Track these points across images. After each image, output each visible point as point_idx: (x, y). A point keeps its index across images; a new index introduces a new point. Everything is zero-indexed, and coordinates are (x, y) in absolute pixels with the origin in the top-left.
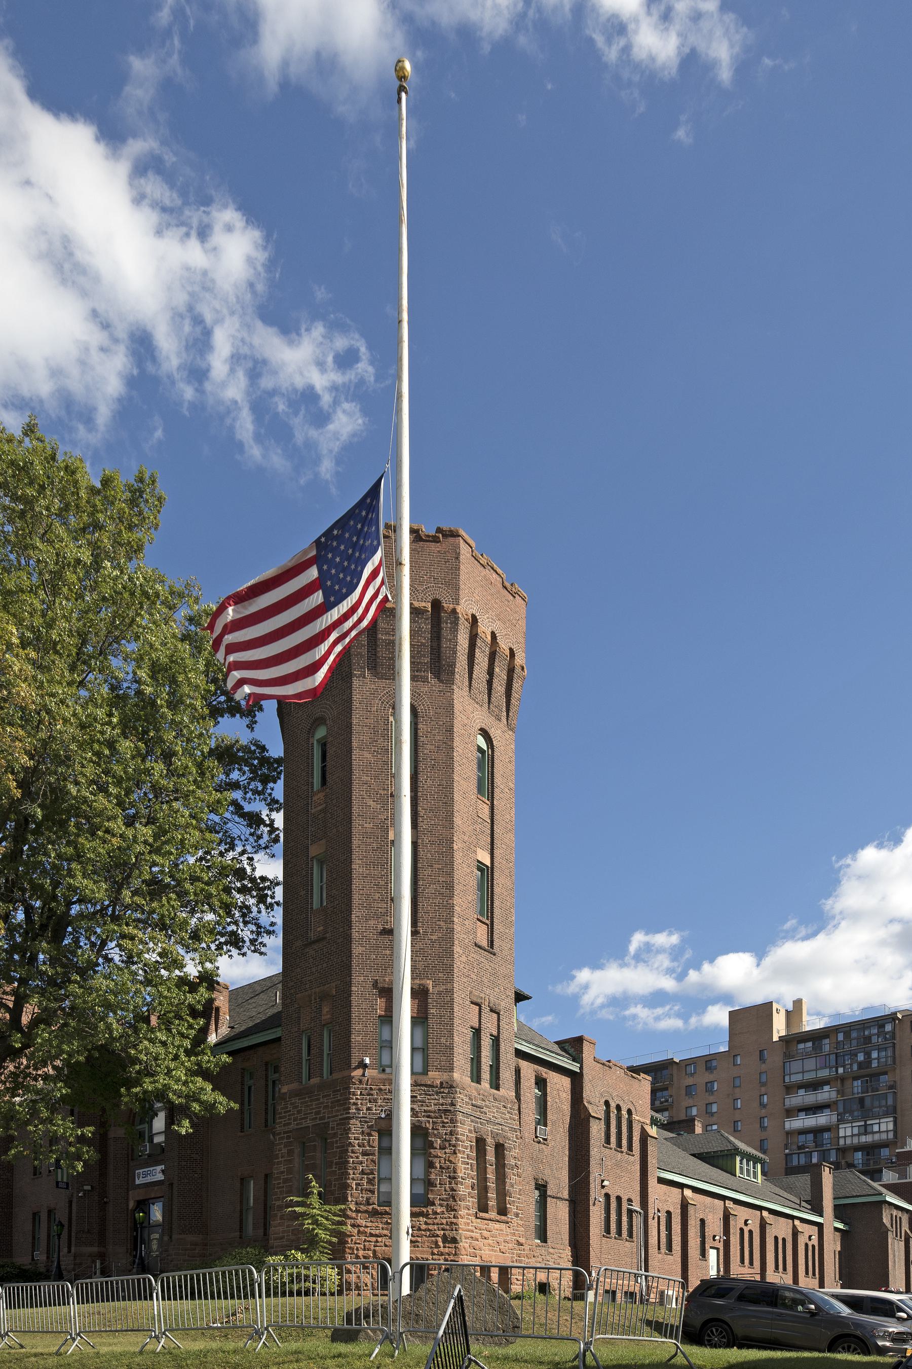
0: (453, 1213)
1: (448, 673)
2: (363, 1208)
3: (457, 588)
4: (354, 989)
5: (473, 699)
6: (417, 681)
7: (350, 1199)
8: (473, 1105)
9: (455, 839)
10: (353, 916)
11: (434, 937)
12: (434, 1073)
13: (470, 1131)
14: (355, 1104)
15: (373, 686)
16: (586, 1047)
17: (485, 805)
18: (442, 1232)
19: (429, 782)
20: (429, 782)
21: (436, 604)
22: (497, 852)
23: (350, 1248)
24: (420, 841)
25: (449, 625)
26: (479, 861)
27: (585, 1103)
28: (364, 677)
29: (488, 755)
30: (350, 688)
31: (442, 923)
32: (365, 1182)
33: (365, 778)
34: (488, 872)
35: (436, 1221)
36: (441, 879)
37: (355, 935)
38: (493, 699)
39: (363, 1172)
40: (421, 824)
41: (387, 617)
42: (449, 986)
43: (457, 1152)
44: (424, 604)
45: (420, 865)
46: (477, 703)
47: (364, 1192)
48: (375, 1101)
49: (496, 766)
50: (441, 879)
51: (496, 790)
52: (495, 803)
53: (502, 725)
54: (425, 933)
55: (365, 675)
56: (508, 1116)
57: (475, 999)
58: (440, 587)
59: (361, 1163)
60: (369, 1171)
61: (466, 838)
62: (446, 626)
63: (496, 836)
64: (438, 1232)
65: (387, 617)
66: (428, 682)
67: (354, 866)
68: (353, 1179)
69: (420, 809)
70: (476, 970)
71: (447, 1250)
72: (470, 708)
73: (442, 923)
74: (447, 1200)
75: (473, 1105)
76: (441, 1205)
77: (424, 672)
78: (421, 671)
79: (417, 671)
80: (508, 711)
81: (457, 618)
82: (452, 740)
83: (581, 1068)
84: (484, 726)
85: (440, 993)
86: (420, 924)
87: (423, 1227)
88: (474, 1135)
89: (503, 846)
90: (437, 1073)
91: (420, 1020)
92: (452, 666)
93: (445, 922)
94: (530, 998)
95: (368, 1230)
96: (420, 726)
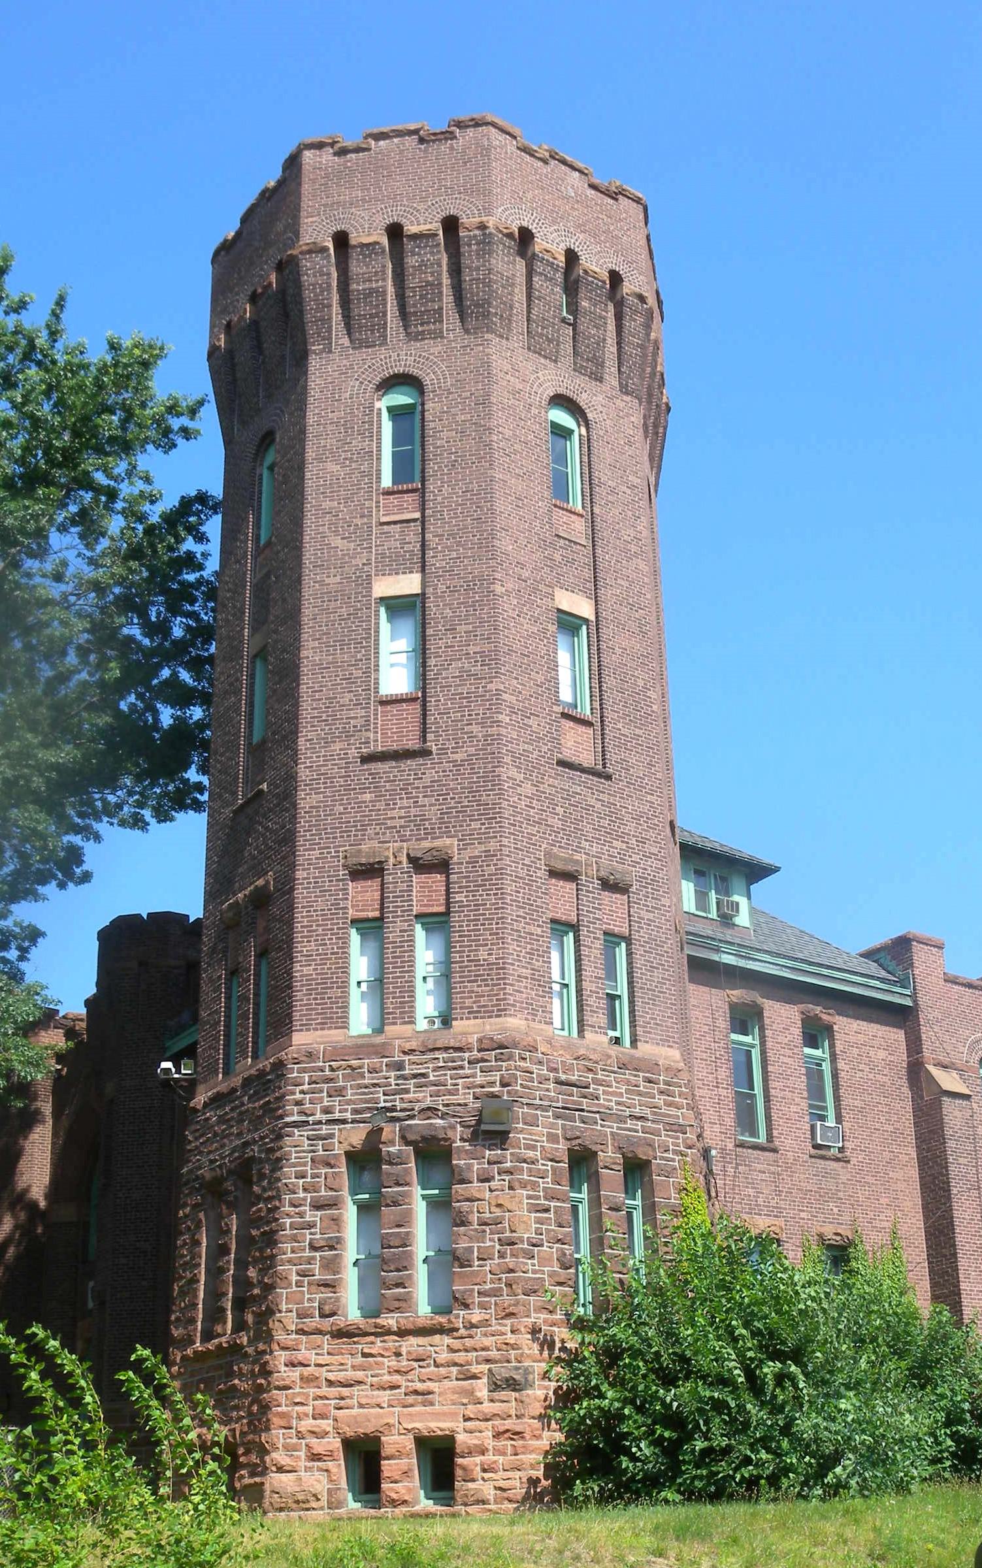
0: (508, 1322)
2: (315, 1322)
4: (300, 874)
5: (535, 352)
6: (423, 339)
7: (284, 1307)
8: (559, 1082)
10: (301, 741)
11: (458, 757)
12: (465, 1022)
13: (553, 1138)
14: (298, 1103)
15: (345, 362)
16: (920, 954)
18: (485, 1367)
20: (446, 490)
23: (282, 1415)
24: (429, 590)
25: (474, 247)
26: (559, 610)
27: (931, 1068)
28: (330, 352)
31: (475, 729)
32: (316, 1267)
33: (327, 504)
35: (468, 1342)
36: (472, 649)
37: (303, 773)
41: (365, 258)
42: (492, 845)
43: (516, 1185)
45: (429, 632)
46: (545, 357)
48: (340, 1092)
49: (595, 451)
53: (605, 387)
54: (443, 751)
56: (660, 1100)
57: (559, 866)
59: (311, 1226)
60: (322, 1243)
61: (526, 574)
63: (600, 566)
64: (475, 1369)
65: (365, 258)
66: (442, 337)
67: (304, 653)
70: (559, 810)
71: (496, 1407)
72: (530, 366)
73: (475, 729)
74: (496, 1293)
75: (559, 1082)
76: (484, 1306)
77: (434, 323)
78: (428, 323)
79: (422, 325)
83: (913, 997)
85: (473, 861)
86: (430, 736)
87: (444, 1356)
88: (562, 1146)
90: (472, 1022)
92: (482, 306)
93: (483, 724)
94: (777, 869)
95: (323, 1373)
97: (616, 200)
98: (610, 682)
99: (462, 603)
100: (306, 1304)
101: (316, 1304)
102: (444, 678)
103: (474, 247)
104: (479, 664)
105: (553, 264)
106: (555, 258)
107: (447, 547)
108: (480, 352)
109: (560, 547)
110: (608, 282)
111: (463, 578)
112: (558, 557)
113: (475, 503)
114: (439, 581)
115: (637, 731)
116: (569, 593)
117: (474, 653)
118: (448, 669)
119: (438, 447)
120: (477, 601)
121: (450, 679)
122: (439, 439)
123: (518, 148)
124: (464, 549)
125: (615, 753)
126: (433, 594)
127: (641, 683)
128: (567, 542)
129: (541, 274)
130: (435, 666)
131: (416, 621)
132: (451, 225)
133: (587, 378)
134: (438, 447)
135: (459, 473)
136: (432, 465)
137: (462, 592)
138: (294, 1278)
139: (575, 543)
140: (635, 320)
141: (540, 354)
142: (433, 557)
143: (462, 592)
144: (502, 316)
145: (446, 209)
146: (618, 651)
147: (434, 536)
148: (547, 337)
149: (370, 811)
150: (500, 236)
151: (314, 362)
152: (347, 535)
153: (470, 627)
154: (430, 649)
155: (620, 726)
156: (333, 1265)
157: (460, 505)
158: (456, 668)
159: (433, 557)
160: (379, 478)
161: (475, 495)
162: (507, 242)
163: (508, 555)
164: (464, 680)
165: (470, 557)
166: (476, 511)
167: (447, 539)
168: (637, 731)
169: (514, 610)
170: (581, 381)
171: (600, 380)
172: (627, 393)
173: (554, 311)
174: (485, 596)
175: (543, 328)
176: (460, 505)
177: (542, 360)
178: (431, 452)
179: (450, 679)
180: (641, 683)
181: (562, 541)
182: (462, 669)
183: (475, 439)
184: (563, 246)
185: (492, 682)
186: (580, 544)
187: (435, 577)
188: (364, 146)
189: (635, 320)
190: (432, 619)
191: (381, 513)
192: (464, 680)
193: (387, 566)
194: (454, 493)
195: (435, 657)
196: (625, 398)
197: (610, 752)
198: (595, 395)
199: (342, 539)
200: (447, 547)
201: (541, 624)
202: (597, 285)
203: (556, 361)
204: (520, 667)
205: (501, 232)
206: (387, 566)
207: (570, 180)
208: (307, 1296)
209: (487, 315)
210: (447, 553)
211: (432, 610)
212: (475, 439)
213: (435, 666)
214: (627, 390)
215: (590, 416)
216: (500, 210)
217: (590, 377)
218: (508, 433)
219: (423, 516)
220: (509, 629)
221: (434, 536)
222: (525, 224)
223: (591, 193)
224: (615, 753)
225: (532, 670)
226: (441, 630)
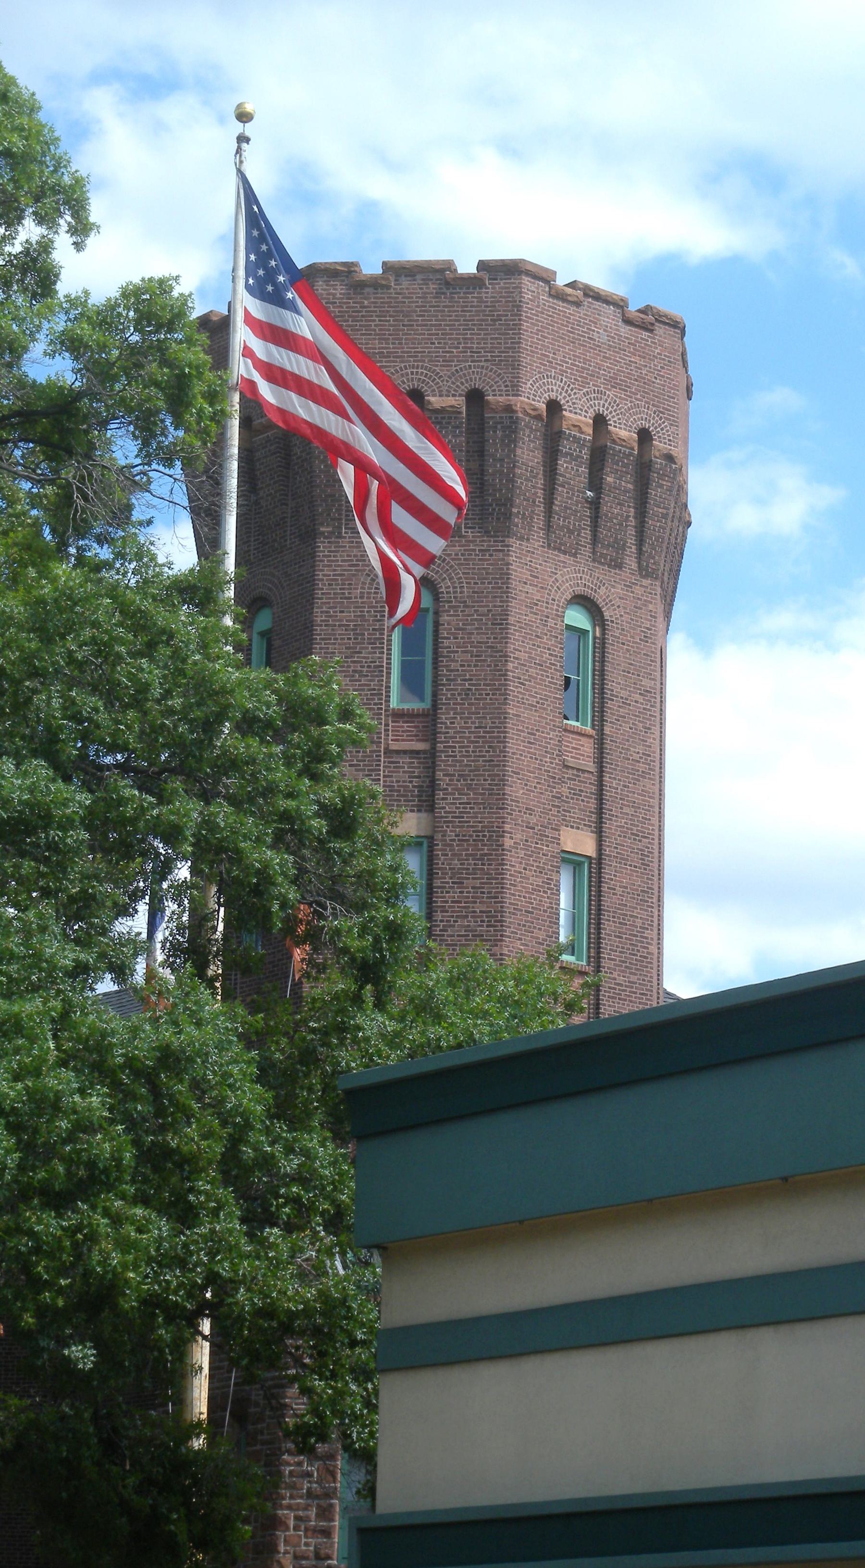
1: (498, 519)
3: (514, 365)
5: (555, 549)
7: (282, 1548)
9: (507, 827)
17: (584, 740)
19: (459, 723)
20: (459, 723)
21: (475, 397)
22: (611, 827)
24: (438, 836)
28: (340, 536)
29: (595, 638)
30: (313, 555)
32: (312, 1513)
34: (590, 868)
36: (478, 908)
38: (603, 532)
39: (310, 1494)
40: (442, 803)
44: (450, 401)
45: (437, 883)
46: (565, 553)
47: (310, 1533)
50: (478, 908)
51: (609, 704)
52: (607, 730)
53: (625, 574)
55: (340, 533)
58: (482, 367)
61: (533, 820)
62: (494, 438)
63: (607, 795)
66: (461, 536)
68: (289, 1507)
69: (440, 774)
80: (640, 542)
81: (515, 422)
82: (504, 639)
84: (580, 590)
89: (626, 810)
91: (272, 240)
96: (444, 618)
97: (651, 331)
98: (608, 927)
99: (471, 855)
100: (304, 1548)
101: (312, 1548)
102: (448, 936)
103: (499, 433)
104: (485, 924)
105: (580, 438)
106: (582, 433)
107: (457, 789)
108: (499, 560)
109: (568, 779)
110: (636, 448)
111: (472, 827)
112: (565, 791)
113: (487, 742)
114: (448, 827)
115: (633, 978)
116: (575, 830)
117: (481, 912)
118: (454, 926)
119: (452, 671)
120: (486, 855)
121: (456, 938)
122: (453, 661)
123: (550, 295)
124: (474, 794)
125: (609, 1006)
126: (442, 840)
127: (639, 922)
128: (575, 772)
129: (567, 454)
130: (442, 921)
131: (421, 857)
132: (475, 397)
133: (606, 568)
134: (452, 671)
135: (472, 704)
136: (444, 692)
137: (471, 842)
138: (292, 1523)
139: (584, 771)
140: (661, 486)
141: (559, 550)
142: (443, 799)
143: (471, 842)
144: (524, 514)
145: (471, 379)
146: (619, 891)
147: (444, 775)
148: (568, 529)
149: (357, 561)
150: (527, 419)
151: (323, 547)
152: (355, 762)
153: (477, 883)
154: (436, 902)
155: (615, 975)
156: (325, 1513)
157: (473, 742)
158: (461, 926)
159: (443, 799)
160: (388, 701)
161: (488, 732)
162: (535, 424)
163: (518, 802)
164: (470, 940)
165: (481, 804)
166: (489, 752)
167: (458, 780)
168: (633, 978)
169: (521, 863)
170: (601, 572)
171: (619, 566)
172: (646, 577)
173: (578, 496)
174: (494, 850)
175: (565, 518)
176: (473, 742)
177: (562, 557)
178: (445, 675)
179: (456, 938)
180: (639, 922)
181: (570, 771)
182: (468, 928)
183: (489, 666)
184: (591, 413)
185: (497, 945)
186: (588, 772)
187: (445, 822)
188: (384, 282)
189: (661, 486)
190: (439, 869)
191: (390, 737)
192: (470, 940)
193: (395, 800)
194: (467, 728)
195: (442, 912)
196: (646, 582)
197: (604, 1005)
198: (613, 587)
199: (350, 766)
200: (457, 789)
201: (546, 874)
202: (624, 453)
203: (575, 555)
204: (524, 926)
205: (528, 415)
206: (395, 800)
207: (604, 320)
208: (304, 1540)
209: (508, 516)
210: (457, 796)
211: (440, 859)
212: (489, 666)
213: (442, 921)
214: (647, 571)
215: (607, 615)
216: (529, 385)
217: (610, 566)
218: (523, 656)
219: (433, 748)
220: (515, 886)
221: (444, 775)
222: (553, 395)
223: (625, 330)
224: (609, 1006)
225: (535, 928)
226: (448, 883)
